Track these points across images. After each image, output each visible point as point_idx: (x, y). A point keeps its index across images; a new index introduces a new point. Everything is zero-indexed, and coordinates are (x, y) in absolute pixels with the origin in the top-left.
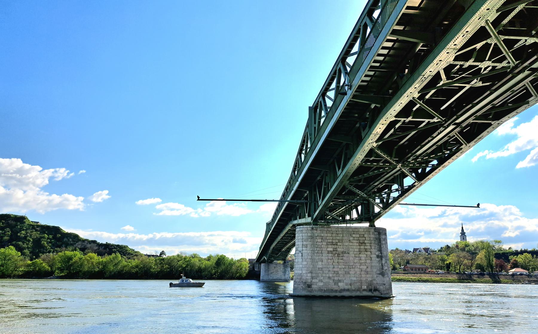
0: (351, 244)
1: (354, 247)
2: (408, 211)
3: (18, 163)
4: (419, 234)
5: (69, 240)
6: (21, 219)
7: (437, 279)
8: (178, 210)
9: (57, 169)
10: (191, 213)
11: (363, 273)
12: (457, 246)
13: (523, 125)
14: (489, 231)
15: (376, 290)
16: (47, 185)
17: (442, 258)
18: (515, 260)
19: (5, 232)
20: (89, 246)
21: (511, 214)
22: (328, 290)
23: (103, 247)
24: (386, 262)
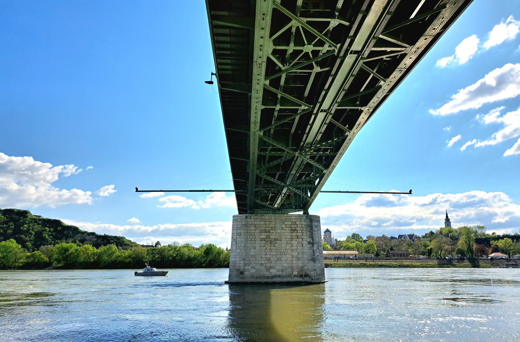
0: (283, 231)
1: (287, 234)
2: (400, 199)
3: (30, 160)
4: (412, 221)
5: (69, 233)
6: (24, 214)
7: (418, 264)
8: (180, 202)
9: (67, 166)
10: (192, 205)
11: (294, 259)
12: (441, 232)
13: (509, 114)
14: (479, 217)
15: (306, 275)
16: (57, 181)
17: (425, 244)
18: (496, 245)
19: (9, 226)
20: (88, 238)
21: (501, 200)
22: (260, 277)
23: (101, 239)
24: (318, 248)
